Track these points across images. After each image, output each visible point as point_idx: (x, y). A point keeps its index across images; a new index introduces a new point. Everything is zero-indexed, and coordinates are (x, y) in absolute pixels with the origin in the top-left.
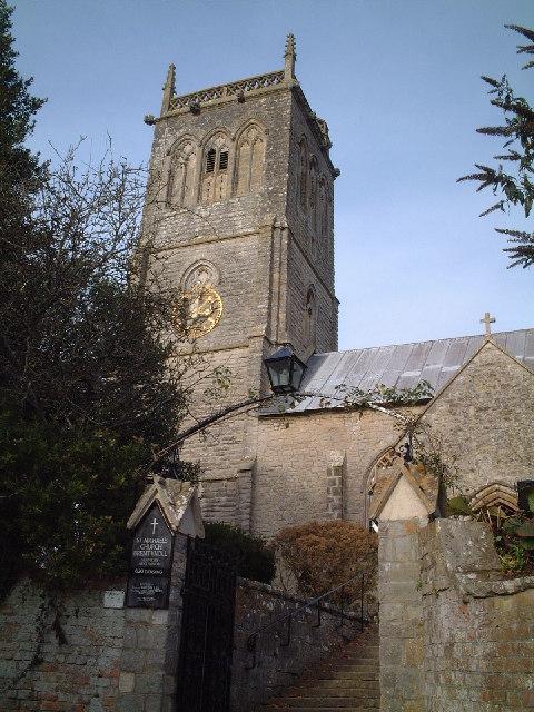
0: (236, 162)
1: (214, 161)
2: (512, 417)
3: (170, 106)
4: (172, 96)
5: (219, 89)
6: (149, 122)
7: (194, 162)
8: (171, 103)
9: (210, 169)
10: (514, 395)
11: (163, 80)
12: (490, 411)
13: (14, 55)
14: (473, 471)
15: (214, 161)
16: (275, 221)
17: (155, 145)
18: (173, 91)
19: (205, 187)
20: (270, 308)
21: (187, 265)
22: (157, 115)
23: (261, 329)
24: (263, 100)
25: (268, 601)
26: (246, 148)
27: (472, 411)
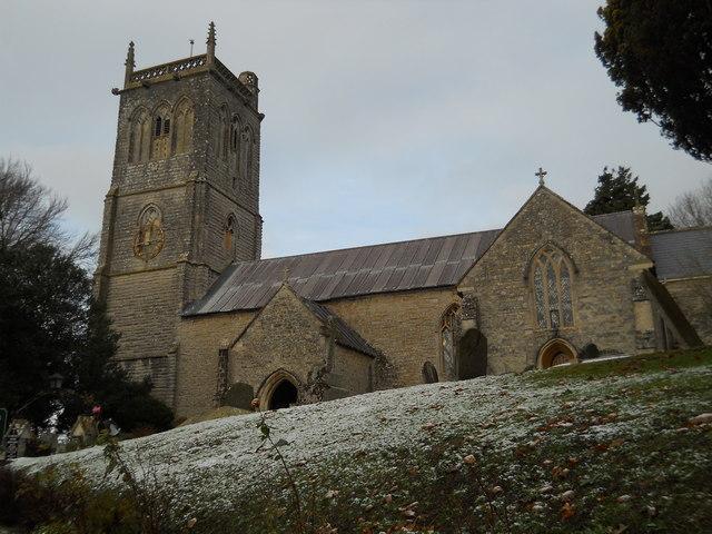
7: (147, 127)
9: (158, 133)
15: (160, 127)
16: (198, 177)
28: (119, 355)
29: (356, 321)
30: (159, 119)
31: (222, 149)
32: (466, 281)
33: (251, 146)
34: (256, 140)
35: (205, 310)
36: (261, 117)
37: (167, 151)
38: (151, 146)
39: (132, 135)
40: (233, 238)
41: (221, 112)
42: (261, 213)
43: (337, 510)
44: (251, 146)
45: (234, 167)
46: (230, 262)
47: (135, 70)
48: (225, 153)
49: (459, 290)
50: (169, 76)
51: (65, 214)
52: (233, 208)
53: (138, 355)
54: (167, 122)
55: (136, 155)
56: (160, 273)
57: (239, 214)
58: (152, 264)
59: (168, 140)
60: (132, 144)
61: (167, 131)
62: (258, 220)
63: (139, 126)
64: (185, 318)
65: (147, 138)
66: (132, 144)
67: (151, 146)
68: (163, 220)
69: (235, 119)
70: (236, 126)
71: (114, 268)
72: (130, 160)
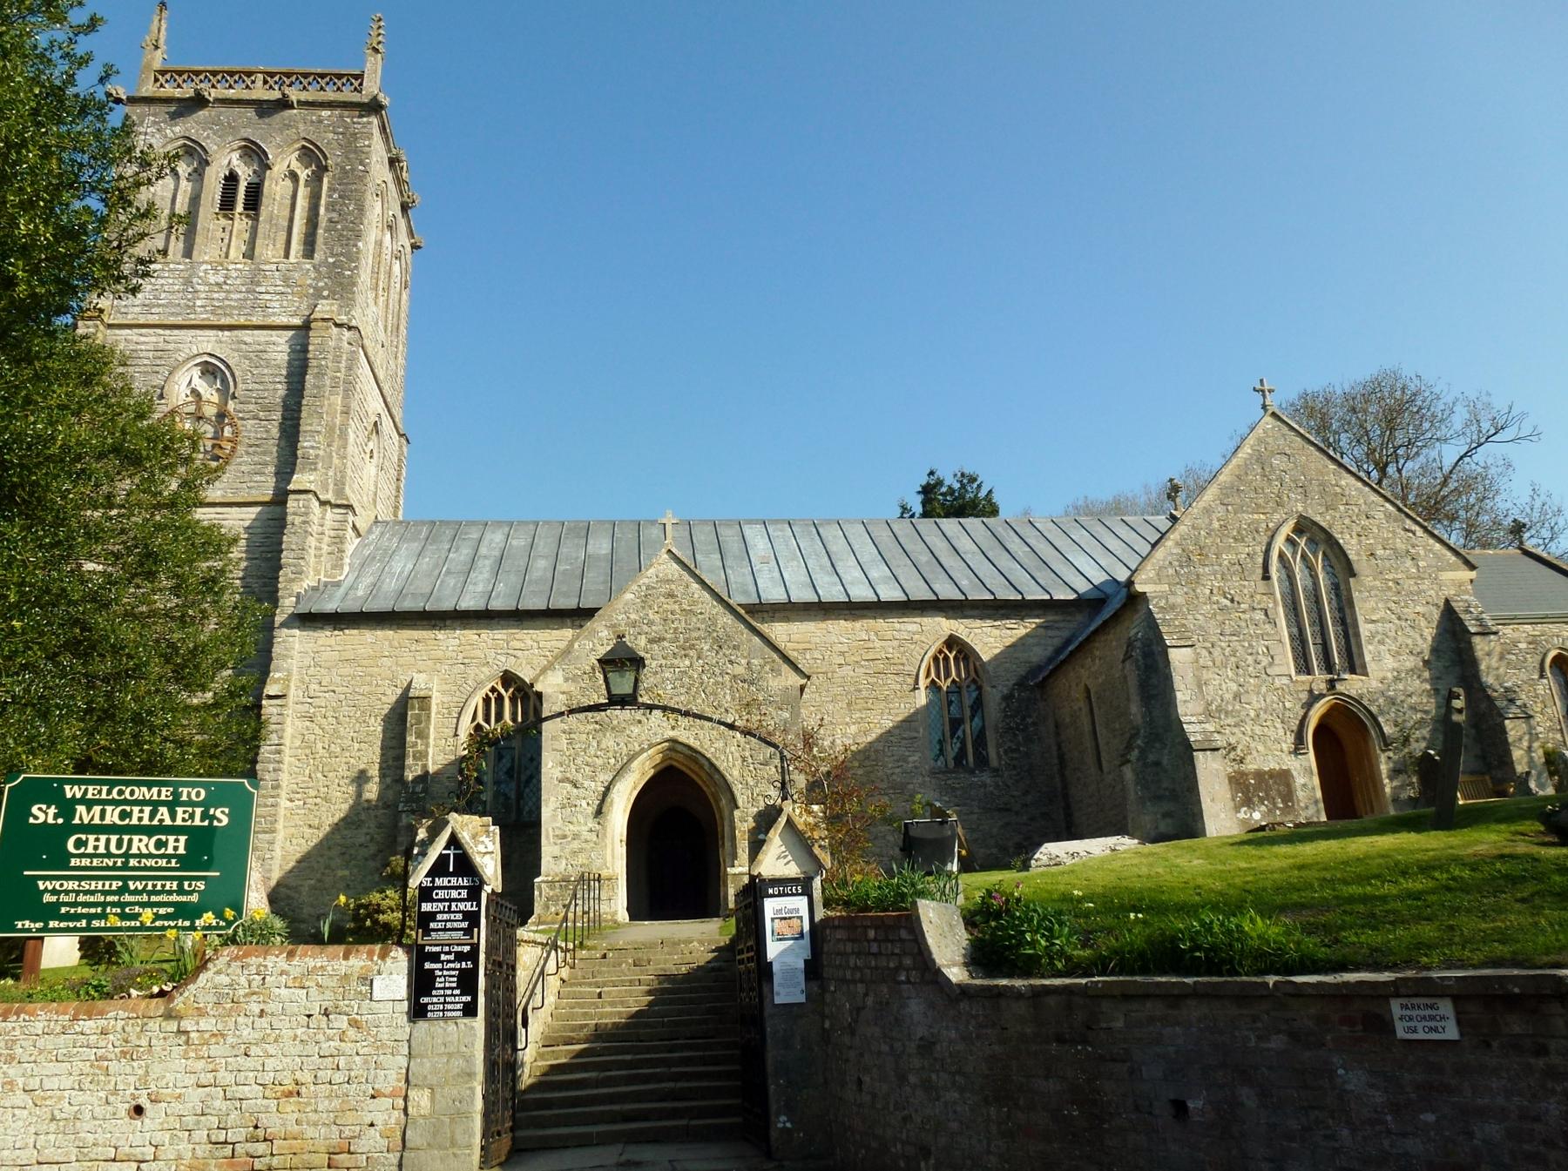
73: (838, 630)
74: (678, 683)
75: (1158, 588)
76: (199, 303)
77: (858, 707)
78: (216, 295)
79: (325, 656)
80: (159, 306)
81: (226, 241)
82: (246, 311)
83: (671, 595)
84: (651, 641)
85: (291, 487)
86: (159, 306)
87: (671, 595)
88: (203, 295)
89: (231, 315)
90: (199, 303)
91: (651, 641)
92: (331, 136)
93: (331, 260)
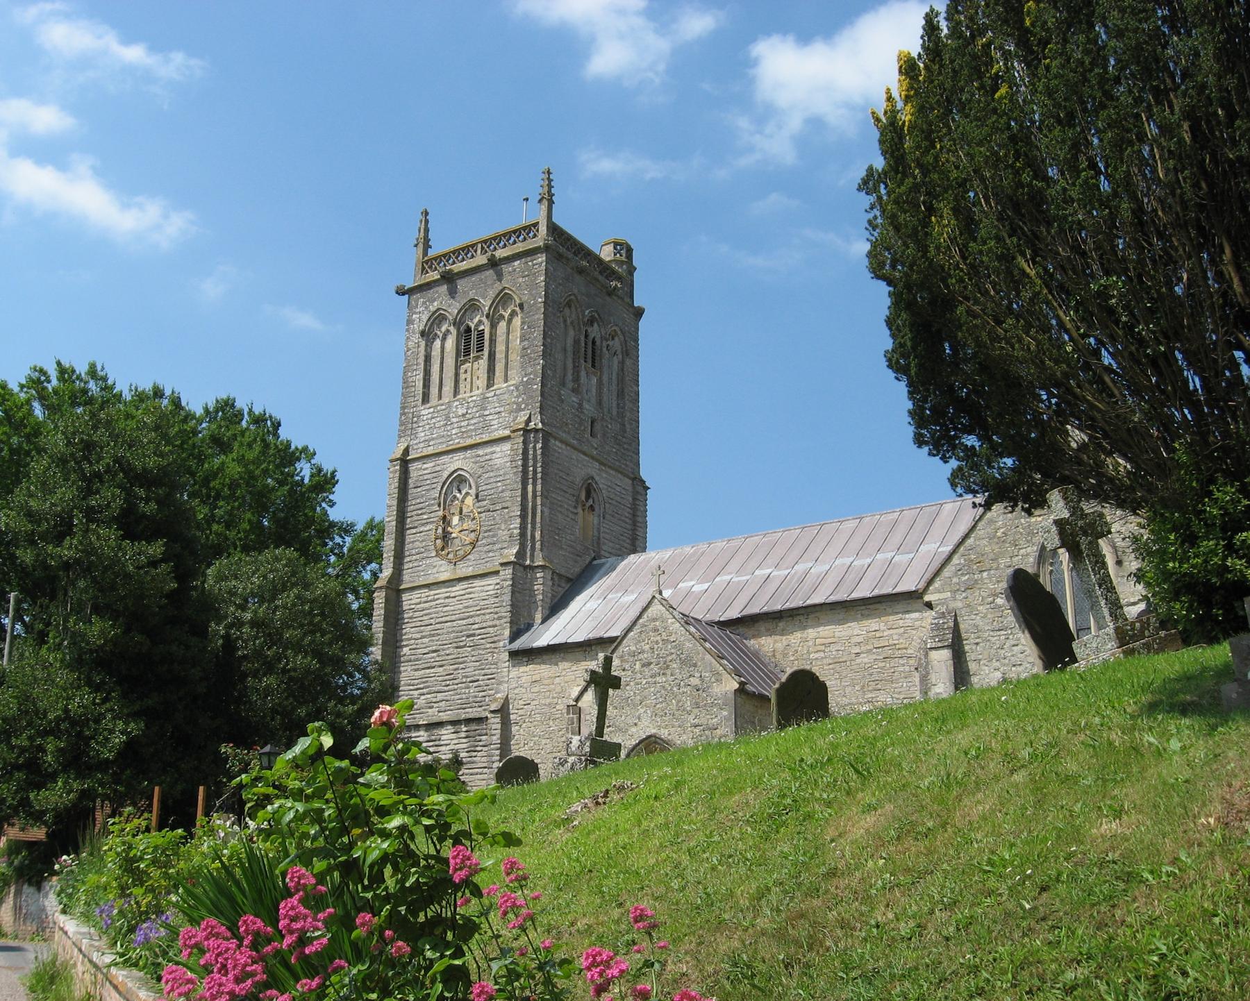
0: (493, 341)
1: (470, 344)
2: (669, 672)
3: (423, 268)
4: (425, 253)
5: (473, 246)
6: (401, 292)
7: (450, 343)
8: (427, 264)
9: (467, 353)
10: (673, 651)
11: (414, 234)
12: (652, 666)
13: (217, 401)
14: (636, 724)
15: (470, 344)
16: (529, 420)
17: (410, 322)
18: (427, 246)
19: (462, 376)
20: (523, 527)
21: (446, 474)
22: (409, 284)
23: (511, 553)
24: (517, 263)
25: (1174, 568)
26: (503, 325)
27: (638, 666)
28: (26, 886)
29: (785, 655)
30: (468, 330)
31: (570, 372)
32: (937, 584)
33: (622, 363)
34: (630, 350)
35: (542, 642)
36: (639, 313)
37: (481, 382)
38: (457, 375)
39: (428, 359)
40: (593, 519)
41: (567, 311)
42: (644, 474)
43: (300, 651)
44: (622, 363)
45: (593, 400)
46: (588, 559)
47: (432, 253)
48: (576, 379)
49: (927, 598)
50: (481, 260)
51: (338, 494)
52: (593, 469)
53: (444, 717)
54: (481, 334)
55: (434, 390)
56: (477, 583)
57: (603, 479)
58: (465, 569)
59: (483, 363)
60: (427, 373)
61: (480, 349)
62: (640, 487)
63: (438, 343)
64: (514, 655)
65: (450, 361)
66: (427, 373)
67: (457, 375)
68: (477, 496)
69: (591, 321)
70: (595, 331)
71: (408, 580)
72: (426, 398)
73: (856, 630)
74: (658, 695)
75: (942, 596)
76: (454, 432)
77: (870, 688)
78: (463, 424)
79: (523, 679)
80: (433, 439)
81: (469, 380)
82: (479, 431)
83: (656, 630)
84: (643, 666)
85: (401, 587)
86: (433, 439)
87: (656, 630)
88: (456, 425)
89: (471, 437)
90: (454, 432)
91: (643, 666)
92: (520, 280)
93: (525, 379)
